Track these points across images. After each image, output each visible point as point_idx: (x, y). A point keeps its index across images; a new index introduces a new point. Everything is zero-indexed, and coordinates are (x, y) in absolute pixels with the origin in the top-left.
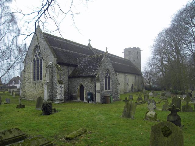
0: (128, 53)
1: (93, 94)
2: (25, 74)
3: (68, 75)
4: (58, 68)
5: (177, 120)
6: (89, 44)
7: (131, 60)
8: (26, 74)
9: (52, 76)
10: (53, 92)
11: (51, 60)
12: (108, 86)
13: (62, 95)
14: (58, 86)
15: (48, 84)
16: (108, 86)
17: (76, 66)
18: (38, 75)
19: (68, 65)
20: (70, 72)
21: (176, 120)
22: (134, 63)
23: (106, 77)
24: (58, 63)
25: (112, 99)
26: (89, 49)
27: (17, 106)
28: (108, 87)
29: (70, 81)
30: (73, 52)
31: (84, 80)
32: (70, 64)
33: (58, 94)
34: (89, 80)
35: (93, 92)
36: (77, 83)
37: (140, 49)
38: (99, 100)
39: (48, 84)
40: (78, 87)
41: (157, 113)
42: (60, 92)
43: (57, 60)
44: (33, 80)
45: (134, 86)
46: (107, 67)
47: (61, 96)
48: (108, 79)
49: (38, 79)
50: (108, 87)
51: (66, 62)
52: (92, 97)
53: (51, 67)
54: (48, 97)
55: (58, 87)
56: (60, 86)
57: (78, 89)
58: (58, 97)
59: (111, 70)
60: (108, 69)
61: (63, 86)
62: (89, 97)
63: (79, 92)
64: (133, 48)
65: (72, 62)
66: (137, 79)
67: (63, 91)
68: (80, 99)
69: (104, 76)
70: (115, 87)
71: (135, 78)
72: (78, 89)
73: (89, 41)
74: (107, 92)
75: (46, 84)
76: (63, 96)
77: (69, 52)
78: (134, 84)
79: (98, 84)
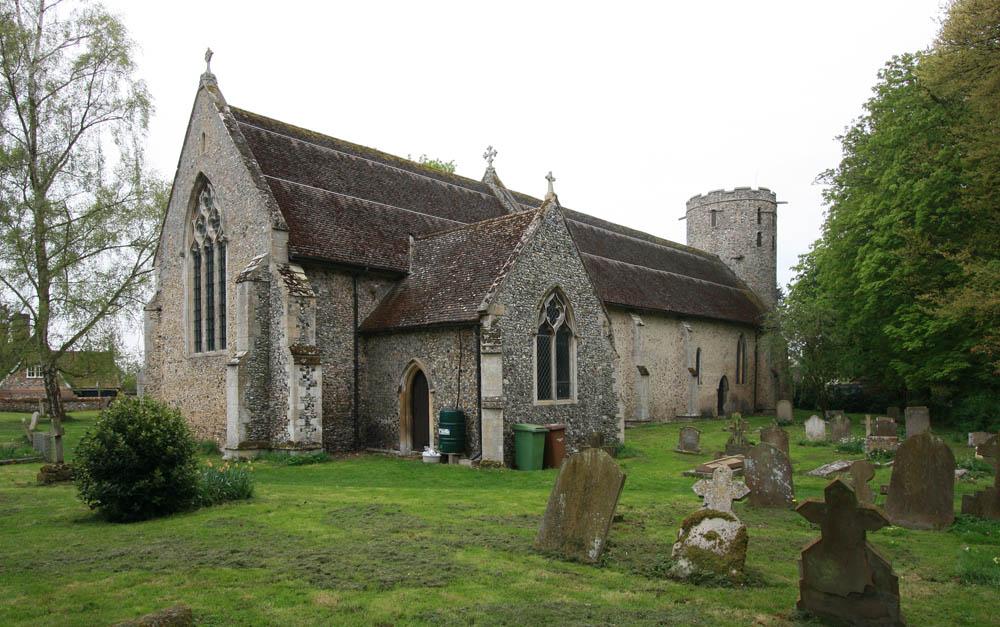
0: (708, 218)
1: (468, 418)
2: (160, 322)
3: (356, 322)
4: (292, 284)
5: (867, 587)
6: (491, 173)
7: (725, 255)
8: (164, 320)
9: (266, 327)
10: (272, 404)
11: (256, 240)
12: (559, 378)
13: (313, 421)
14: (289, 373)
15: (242, 366)
16: (553, 374)
17: (398, 276)
18: (209, 326)
19: (356, 272)
20: (368, 307)
21: (860, 589)
22: (739, 270)
23: (545, 329)
24: (294, 260)
25: (89, 419)
26: (484, 196)
27: (41, 469)
28: (554, 384)
29: (366, 354)
30: (389, 206)
31: (431, 344)
32: (364, 268)
33: (289, 414)
34: (450, 342)
35: (468, 406)
36: (399, 358)
37: (774, 196)
38: (497, 449)
39: (242, 366)
40: (403, 382)
41: (750, 532)
42: (302, 407)
43: (291, 243)
44: (193, 349)
45: (733, 388)
46: (553, 279)
47: (308, 424)
48: (554, 342)
49: (211, 346)
50: (554, 384)
51: (344, 254)
52: (462, 439)
53: (259, 280)
54: (243, 432)
55: (289, 382)
56: (300, 374)
57: (400, 391)
58: (292, 432)
59: (570, 294)
60: (556, 289)
61: (317, 375)
62: (446, 432)
63: (408, 410)
64: (737, 190)
65: (374, 257)
66: (750, 350)
67: (320, 401)
68: (409, 444)
69: (534, 323)
70: (599, 383)
71: (741, 347)
72: (400, 391)
73: (490, 154)
74: (551, 408)
75: (233, 365)
76: (320, 429)
77: (371, 208)
78: (731, 374)
79: (492, 367)
